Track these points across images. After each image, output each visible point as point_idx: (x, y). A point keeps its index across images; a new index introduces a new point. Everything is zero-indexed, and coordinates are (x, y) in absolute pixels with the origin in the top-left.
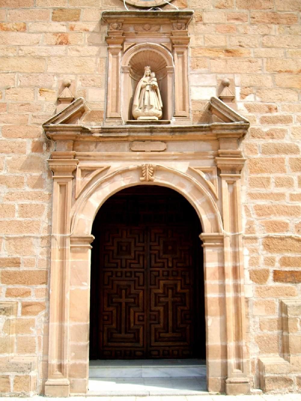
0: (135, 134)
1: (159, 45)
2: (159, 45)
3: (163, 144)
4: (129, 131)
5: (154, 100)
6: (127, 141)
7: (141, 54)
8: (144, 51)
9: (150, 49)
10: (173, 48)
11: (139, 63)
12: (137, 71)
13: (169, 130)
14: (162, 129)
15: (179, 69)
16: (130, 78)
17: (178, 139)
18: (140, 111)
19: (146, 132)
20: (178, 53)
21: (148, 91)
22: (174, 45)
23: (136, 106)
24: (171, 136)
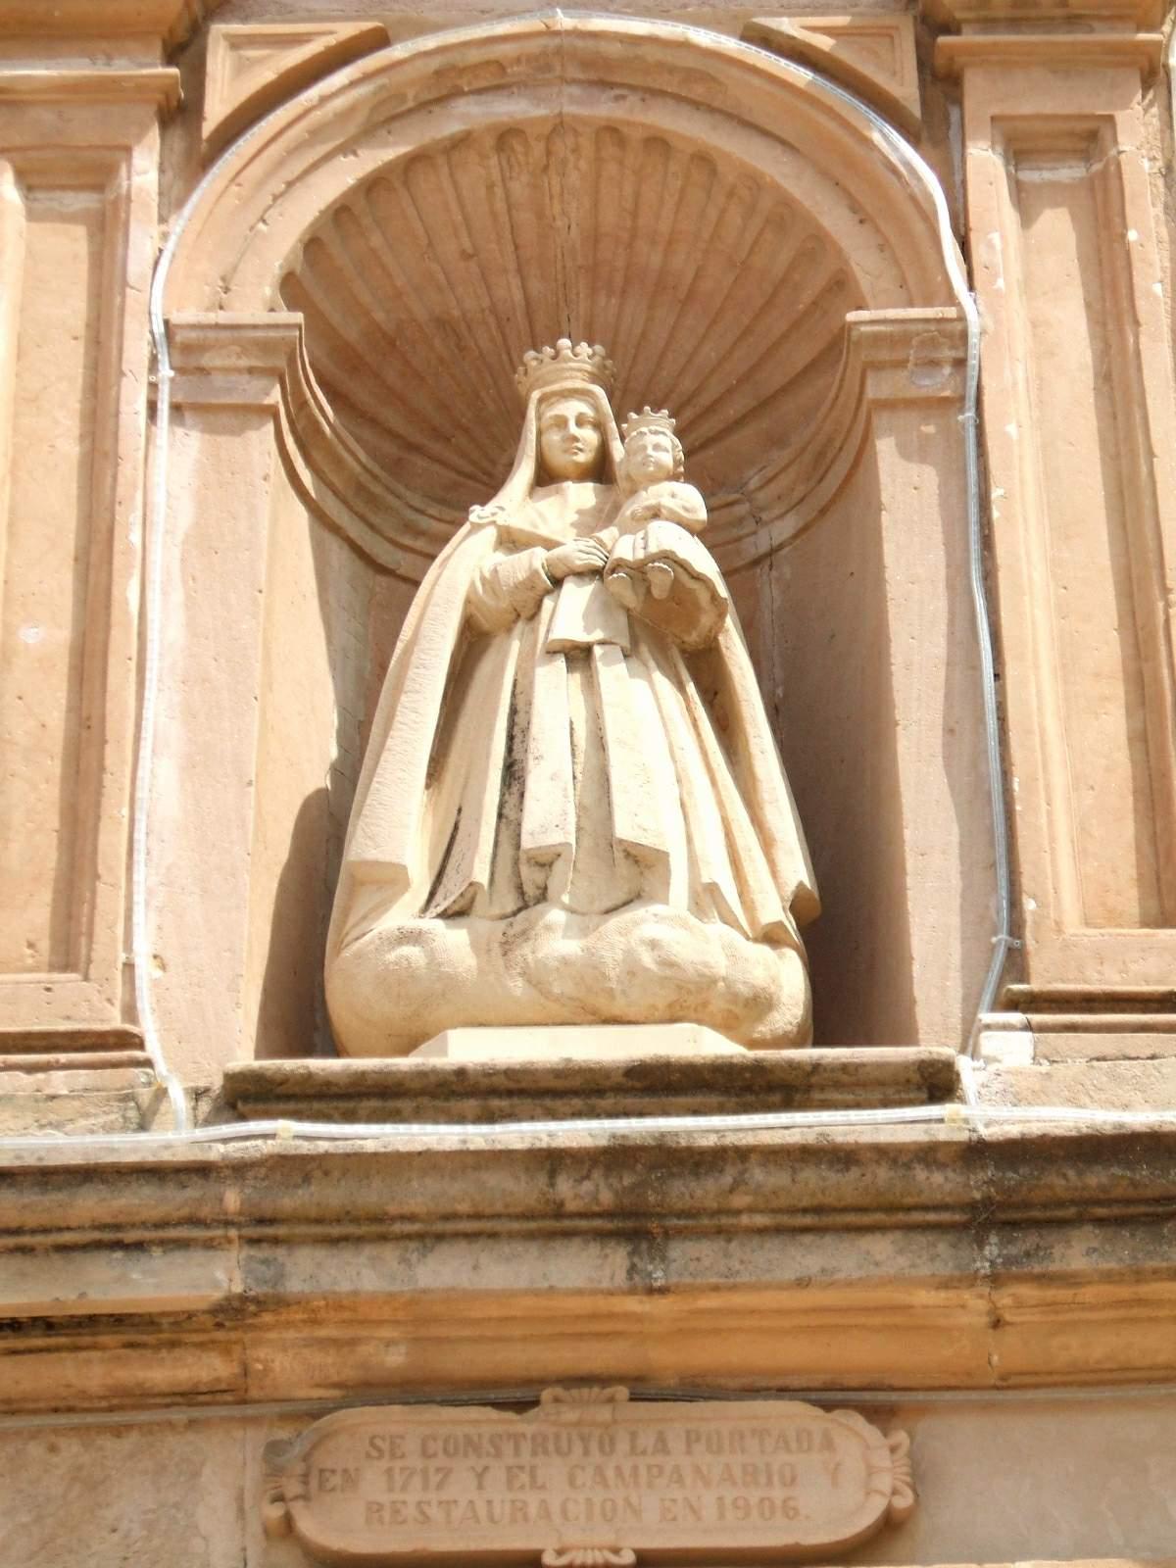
0: (361, 1274)
1: (730, 45)
2: (730, 45)
3: (853, 1433)
4: (263, 1230)
5: (681, 793)
6: (233, 1398)
7: (475, 173)
8: (506, 136)
9: (605, 109)
10: (942, 83)
11: (443, 323)
12: (396, 427)
13: (939, 1183)
14: (814, 1181)
15: (1045, 352)
16: (301, 515)
17: (1102, 1346)
18: (454, 942)
19: (551, 1226)
20: (1020, 149)
21: (579, 656)
22: (951, 28)
23: (392, 879)
24: (975, 1303)
